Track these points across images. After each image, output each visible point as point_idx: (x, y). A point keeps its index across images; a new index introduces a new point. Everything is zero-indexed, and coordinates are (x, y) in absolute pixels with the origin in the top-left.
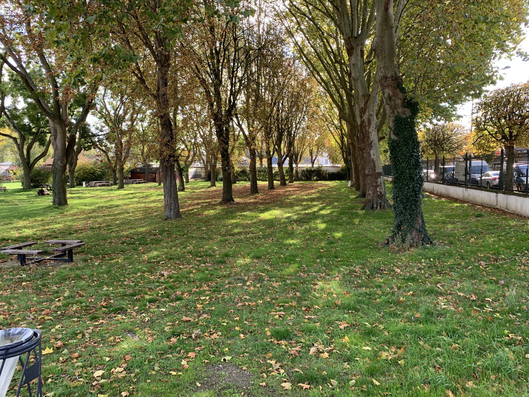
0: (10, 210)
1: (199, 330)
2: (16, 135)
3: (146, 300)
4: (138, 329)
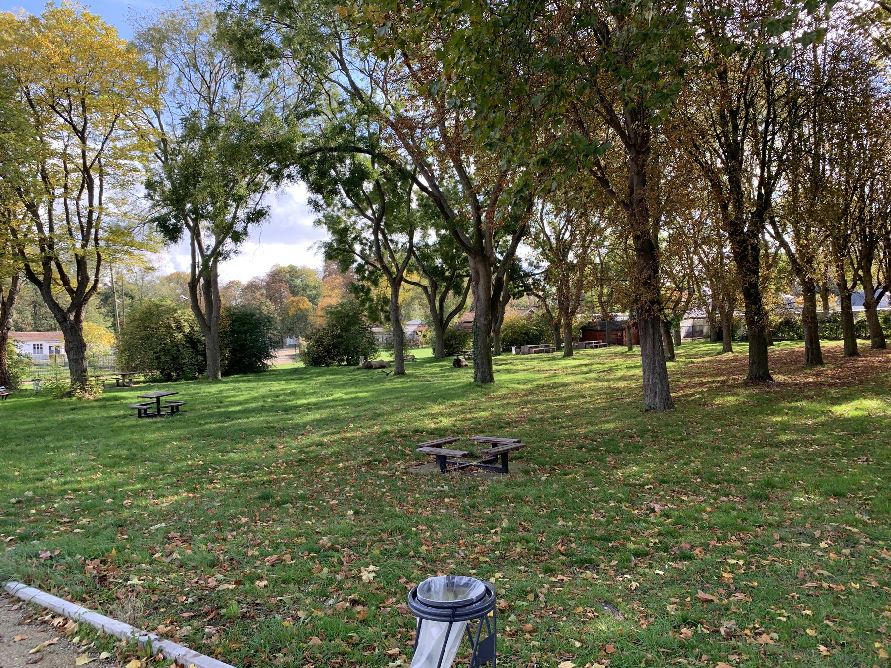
0: (421, 389)
1: (733, 621)
2: (425, 282)
3: (630, 551)
4: (620, 600)
